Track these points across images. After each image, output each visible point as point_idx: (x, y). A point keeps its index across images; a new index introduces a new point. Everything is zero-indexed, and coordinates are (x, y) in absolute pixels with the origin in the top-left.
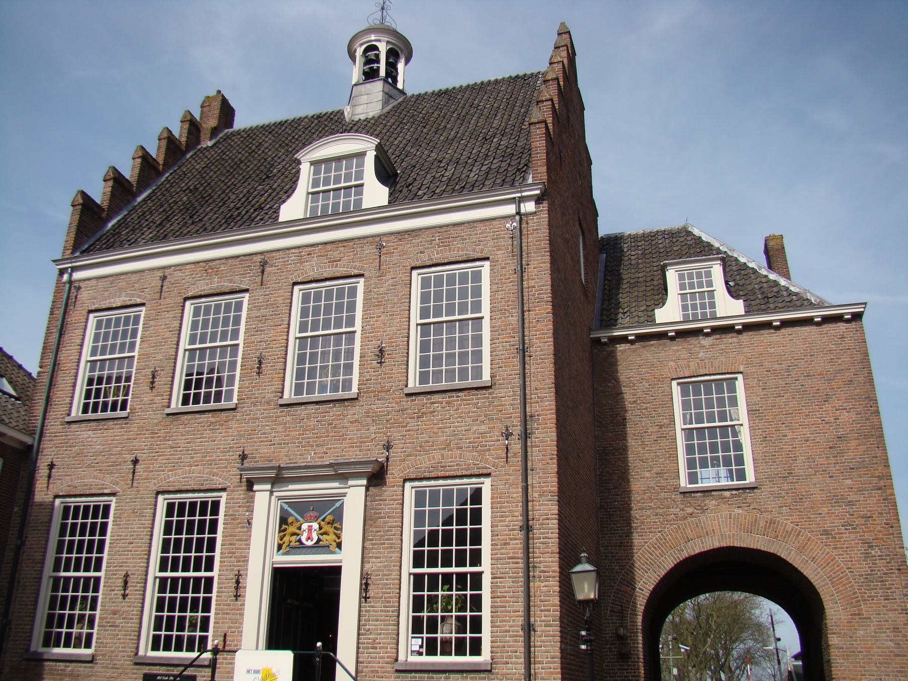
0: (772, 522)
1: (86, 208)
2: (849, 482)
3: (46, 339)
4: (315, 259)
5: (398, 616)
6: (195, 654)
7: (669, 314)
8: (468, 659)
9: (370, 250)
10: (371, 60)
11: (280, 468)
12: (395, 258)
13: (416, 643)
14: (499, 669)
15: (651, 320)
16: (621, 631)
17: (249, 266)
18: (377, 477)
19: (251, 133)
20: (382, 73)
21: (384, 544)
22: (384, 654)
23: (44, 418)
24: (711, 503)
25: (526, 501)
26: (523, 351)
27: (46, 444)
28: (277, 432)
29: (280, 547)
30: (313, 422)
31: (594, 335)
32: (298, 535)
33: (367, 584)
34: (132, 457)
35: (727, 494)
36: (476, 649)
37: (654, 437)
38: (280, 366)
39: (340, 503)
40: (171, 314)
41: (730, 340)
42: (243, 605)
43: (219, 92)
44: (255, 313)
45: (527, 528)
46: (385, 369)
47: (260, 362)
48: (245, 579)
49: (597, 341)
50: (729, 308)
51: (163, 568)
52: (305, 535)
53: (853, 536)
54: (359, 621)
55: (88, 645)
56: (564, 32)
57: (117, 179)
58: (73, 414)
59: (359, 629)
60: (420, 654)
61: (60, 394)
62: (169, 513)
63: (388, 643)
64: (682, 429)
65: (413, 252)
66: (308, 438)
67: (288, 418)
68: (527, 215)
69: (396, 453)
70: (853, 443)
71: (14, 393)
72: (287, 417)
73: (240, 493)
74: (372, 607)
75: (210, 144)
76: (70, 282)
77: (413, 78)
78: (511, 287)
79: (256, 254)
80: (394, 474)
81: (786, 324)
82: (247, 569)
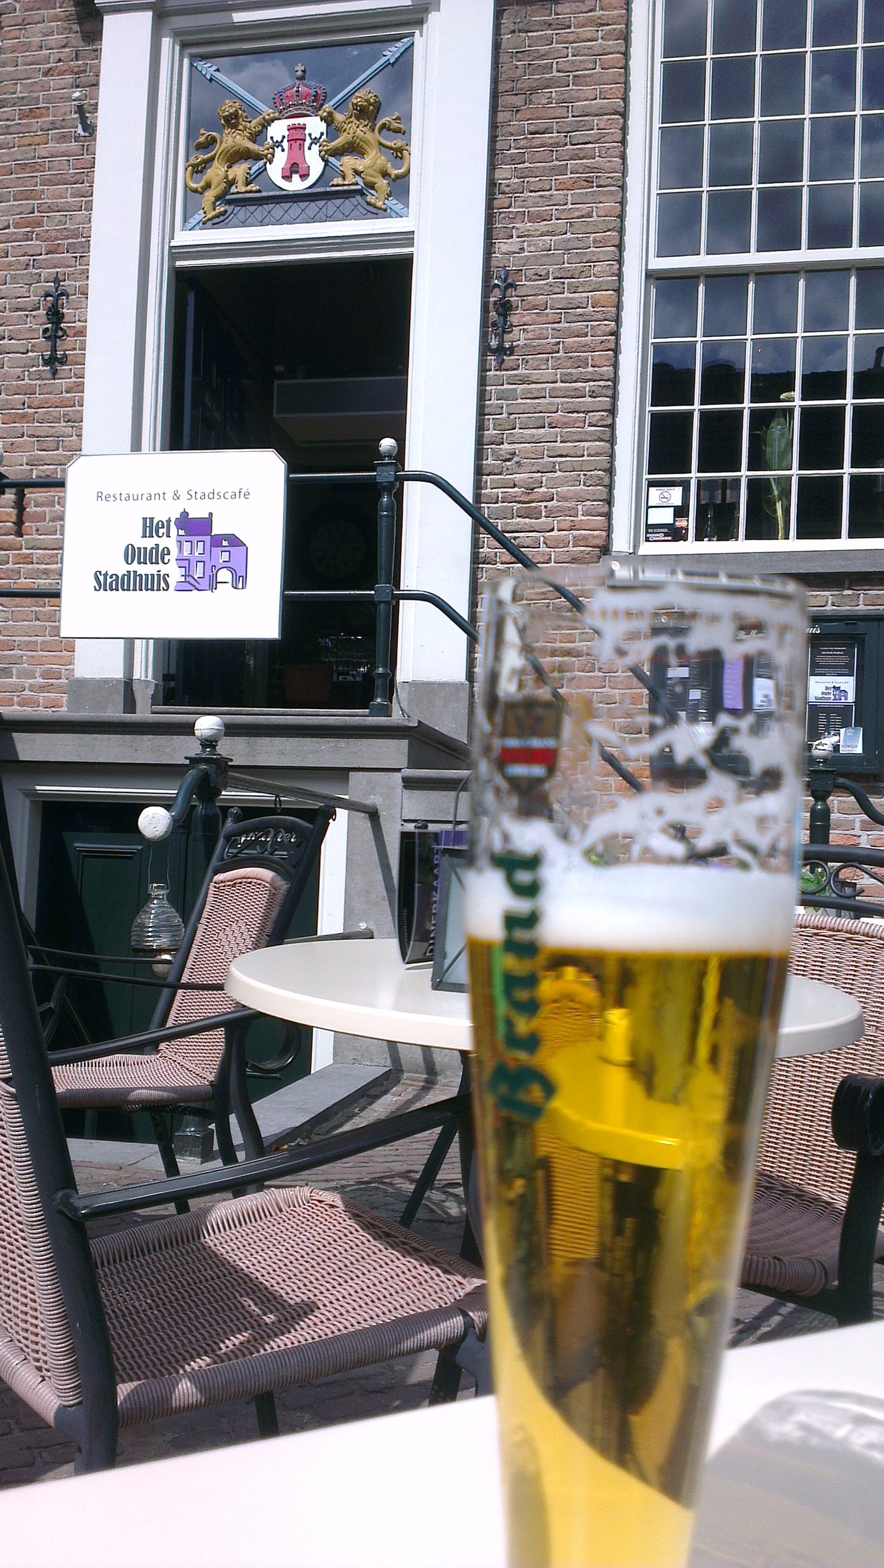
5: (613, 411)
13: (664, 503)
21: (562, 170)
32: (257, 157)
39: (401, 46)
42: (79, 387)
48: (82, 307)
52: (281, 158)
54: (481, 427)
59: (479, 454)
60: (676, 534)
64: (651, 276)
82: (85, 274)
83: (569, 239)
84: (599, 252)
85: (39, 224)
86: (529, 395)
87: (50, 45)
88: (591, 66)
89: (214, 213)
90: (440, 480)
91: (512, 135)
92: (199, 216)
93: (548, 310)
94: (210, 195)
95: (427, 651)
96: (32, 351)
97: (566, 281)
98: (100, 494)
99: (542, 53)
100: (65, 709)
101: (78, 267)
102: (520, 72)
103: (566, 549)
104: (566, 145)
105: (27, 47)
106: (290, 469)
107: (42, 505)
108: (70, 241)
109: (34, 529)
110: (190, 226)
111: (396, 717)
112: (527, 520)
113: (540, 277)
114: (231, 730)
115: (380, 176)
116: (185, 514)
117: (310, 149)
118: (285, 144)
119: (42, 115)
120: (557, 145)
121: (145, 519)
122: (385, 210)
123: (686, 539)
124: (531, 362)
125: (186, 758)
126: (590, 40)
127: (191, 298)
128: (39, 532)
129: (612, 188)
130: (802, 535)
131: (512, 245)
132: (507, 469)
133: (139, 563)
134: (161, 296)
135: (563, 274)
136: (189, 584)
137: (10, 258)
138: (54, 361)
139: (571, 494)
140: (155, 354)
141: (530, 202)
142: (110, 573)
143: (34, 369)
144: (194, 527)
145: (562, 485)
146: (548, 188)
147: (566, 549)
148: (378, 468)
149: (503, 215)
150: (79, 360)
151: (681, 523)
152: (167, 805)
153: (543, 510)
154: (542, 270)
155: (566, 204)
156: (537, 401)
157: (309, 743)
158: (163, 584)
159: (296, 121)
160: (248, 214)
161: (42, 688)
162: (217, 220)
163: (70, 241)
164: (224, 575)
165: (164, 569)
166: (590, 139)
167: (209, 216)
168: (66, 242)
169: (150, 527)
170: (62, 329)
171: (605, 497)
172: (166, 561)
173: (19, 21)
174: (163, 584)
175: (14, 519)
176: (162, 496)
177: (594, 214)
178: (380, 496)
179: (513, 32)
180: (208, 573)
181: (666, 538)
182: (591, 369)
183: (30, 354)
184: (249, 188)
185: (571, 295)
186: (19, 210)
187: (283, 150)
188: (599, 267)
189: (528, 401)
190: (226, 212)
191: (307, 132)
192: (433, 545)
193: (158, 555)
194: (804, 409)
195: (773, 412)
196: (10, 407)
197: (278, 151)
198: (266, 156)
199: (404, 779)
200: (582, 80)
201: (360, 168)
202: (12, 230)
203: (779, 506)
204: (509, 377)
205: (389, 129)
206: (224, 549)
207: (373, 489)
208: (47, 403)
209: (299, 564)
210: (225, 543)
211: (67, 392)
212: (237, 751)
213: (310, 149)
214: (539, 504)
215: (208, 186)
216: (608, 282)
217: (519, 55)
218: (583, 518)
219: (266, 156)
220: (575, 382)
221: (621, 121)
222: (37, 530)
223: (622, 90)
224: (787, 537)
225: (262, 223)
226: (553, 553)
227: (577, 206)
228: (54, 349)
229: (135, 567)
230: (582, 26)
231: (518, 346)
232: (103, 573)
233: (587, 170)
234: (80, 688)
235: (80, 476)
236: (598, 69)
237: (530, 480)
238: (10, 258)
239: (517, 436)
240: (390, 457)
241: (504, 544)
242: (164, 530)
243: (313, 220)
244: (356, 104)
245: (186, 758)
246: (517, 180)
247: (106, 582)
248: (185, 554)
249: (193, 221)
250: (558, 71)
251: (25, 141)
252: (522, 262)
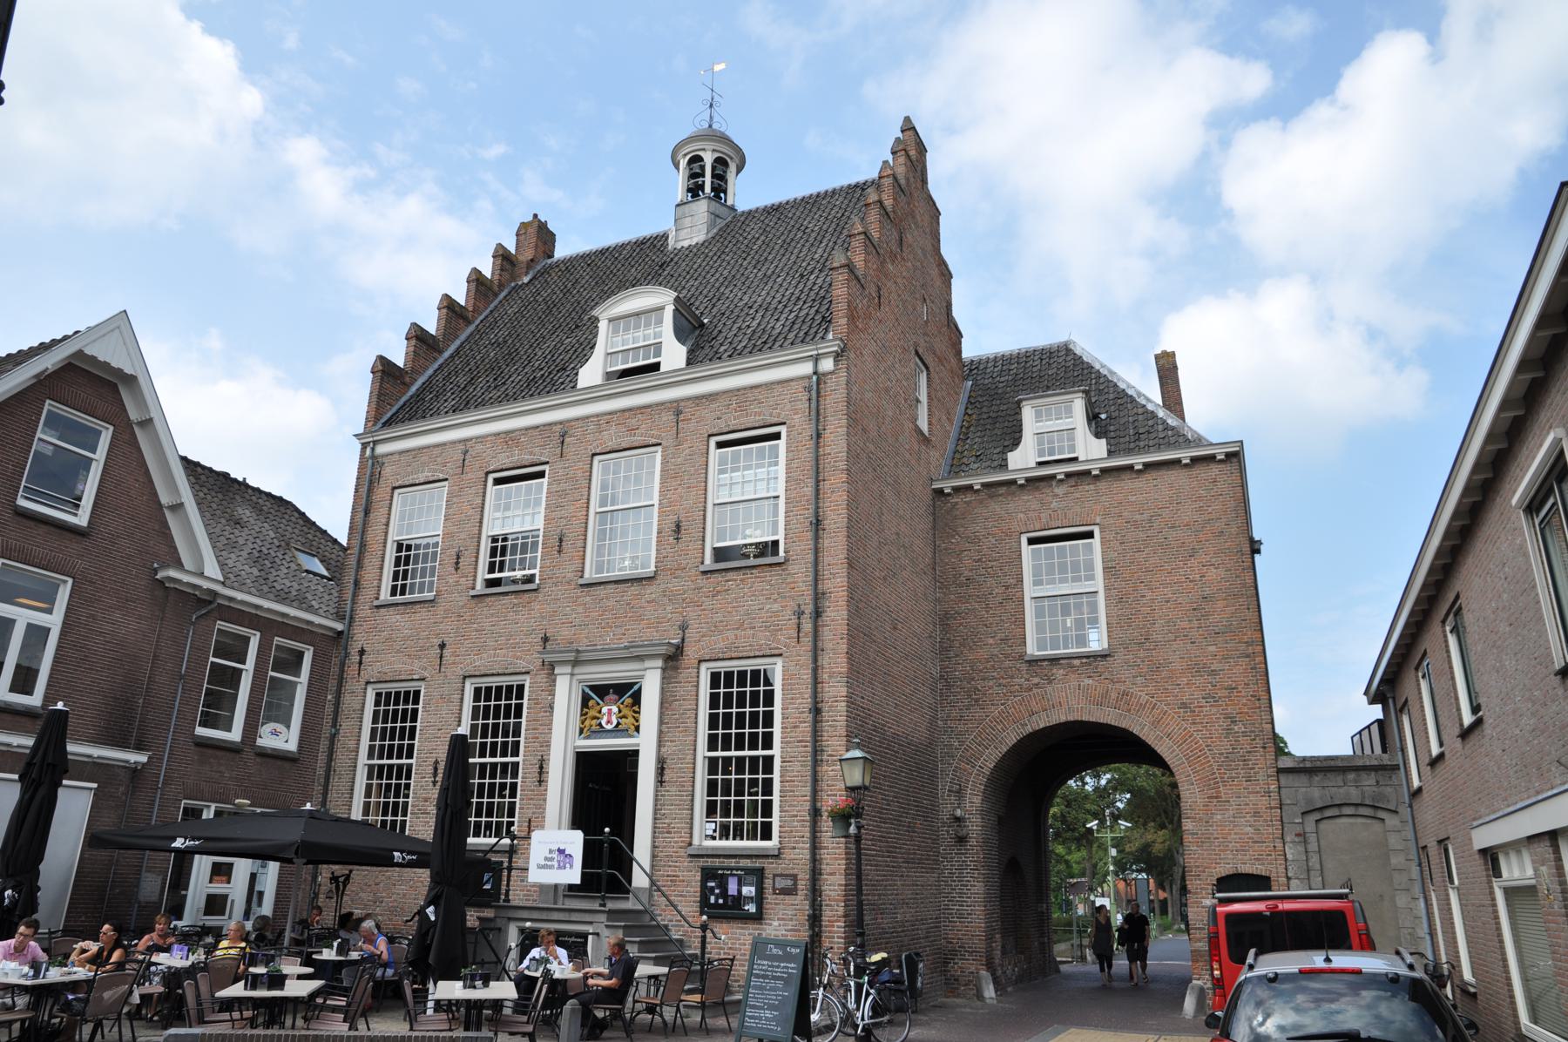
0: (1125, 694)
1: (385, 370)
2: (1212, 648)
3: (352, 519)
6: (493, 840)
7: (1023, 459)
8: (759, 843)
9: (668, 417)
10: (695, 175)
11: (578, 651)
12: (692, 425)
14: (788, 854)
15: (1003, 466)
16: (958, 813)
18: (673, 658)
19: (571, 263)
20: (708, 189)
22: (678, 839)
23: (354, 602)
24: (1059, 673)
25: (816, 681)
26: (817, 524)
27: (356, 630)
29: (581, 731)
30: (611, 603)
31: (936, 486)
33: (662, 769)
34: (437, 641)
35: (1077, 662)
36: (767, 835)
37: (999, 599)
38: (580, 544)
40: (473, 491)
41: (1088, 488)
43: (535, 216)
44: (555, 488)
45: (816, 711)
46: (682, 545)
47: (561, 540)
49: (940, 492)
50: (1092, 450)
51: (712, 745)
53: (1214, 710)
55: (767, 835)
56: (908, 127)
57: (418, 336)
58: (382, 597)
60: (714, 838)
61: (368, 574)
62: (477, 698)
65: (709, 419)
68: (824, 374)
69: (691, 634)
70: (1220, 604)
71: (325, 573)
73: (542, 678)
75: (526, 280)
76: (373, 457)
77: (747, 193)
78: (807, 454)
79: (555, 424)
80: (691, 653)
81: (1147, 466)
136: (559, 868)
144: (561, 851)
157: (826, 559)
169: (551, 851)
193: (552, 859)
209: (586, 863)
247: (540, 867)
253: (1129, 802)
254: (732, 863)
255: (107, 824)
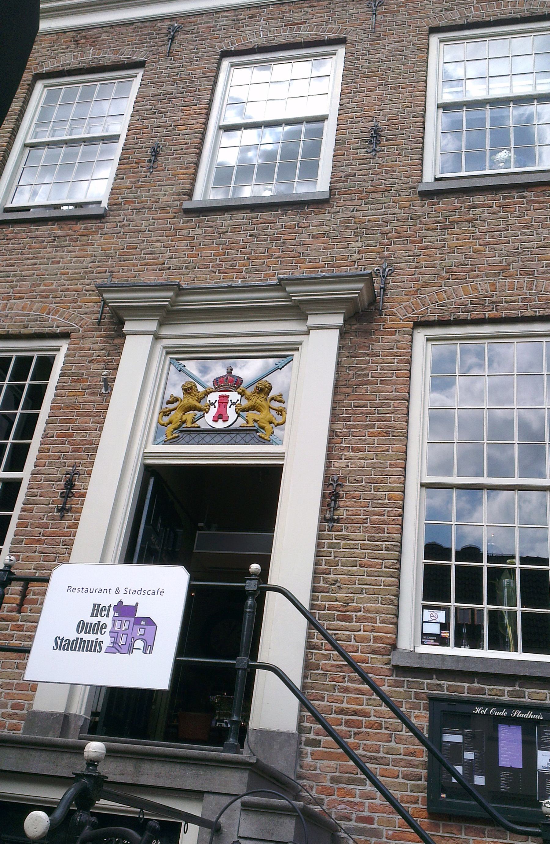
4: (262, 22)
11: (180, 290)
17: (149, 34)
18: (362, 318)
21: (373, 426)
28: (176, 251)
30: (242, 237)
38: (192, 158)
42: (76, 526)
52: (213, 411)
63: (378, 612)
66: (233, 260)
67: (198, 231)
72: (197, 230)
73: (95, 343)
74: (345, 538)
80: (398, 307)
83: (375, 462)
84: (393, 471)
85: (71, 436)
86: (348, 547)
87: (95, 349)
88: (390, 376)
89: (171, 437)
90: (286, 591)
91: (344, 407)
92: (164, 438)
93: (361, 500)
94: (171, 427)
95: (273, 708)
96: (52, 504)
97: (373, 485)
98: (70, 588)
99: (363, 368)
100: (21, 732)
101: (89, 460)
102: (351, 376)
103: (369, 644)
104: (375, 414)
105: (82, 349)
106: (191, 579)
107: (37, 594)
108: (87, 446)
109: (29, 609)
110: (157, 443)
111: (245, 755)
112: (343, 623)
113: (357, 481)
114: (111, 753)
115: (268, 423)
116: (121, 602)
117: (230, 407)
118: (217, 404)
119: (84, 382)
120: (370, 413)
121: (95, 605)
122: (269, 441)
123: (449, 646)
124: (350, 528)
125: (73, 773)
126: (390, 363)
127: (152, 481)
128: (32, 611)
129: (401, 438)
130: (525, 650)
131: (342, 463)
132: (332, 590)
133: (85, 633)
134: (134, 478)
135: (371, 481)
136: (115, 648)
137: (50, 453)
138: (63, 510)
139: (373, 609)
140: (125, 509)
141: (353, 442)
142: (65, 639)
143: (51, 514)
144: (125, 611)
145: (367, 603)
146: (364, 435)
147: (369, 644)
148: (247, 581)
149: (337, 448)
150: (79, 510)
151: (445, 634)
152: (49, 811)
153: (354, 617)
154: (358, 478)
155: (374, 444)
156: (353, 550)
158: (98, 648)
159: (224, 393)
160: (191, 438)
161: (10, 716)
162: (171, 441)
163: (87, 446)
164: (139, 644)
165: (100, 637)
166: (389, 412)
167: (169, 438)
168: (84, 446)
169: (97, 610)
170: (72, 492)
171: (394, 612)
172: (103, 633)
173: (81, 336)
174: (98, 648)
175: (18, 602)
176: (108, 590)
177: (390, 450)
178: (246, 599)
179: (348, 357)
180: (129, 642)
181: (435, 643)
182: (386, 535)
183: (50, 505)
184: (193, 425)
185: (375, 493)
186: (61, 428)
187: (215, 407)
188: (393, 478)
189: (347, 550)
190: (178, 436)
191: (229, 399)
192: (282, 636)
193: (99, 628)
194: (522, 570)
195: (502, 570)
196: (31, 535)
197: (212, 407)
198: (205, 410)
199: (244, 804)
200: (384, 382)
201: (257, 419)
202: (55, 438)
203: (509, 630)
204: (336, 536)
205: (275, 401)
206: (142, 627)
207: (243, 594)
208: (54, 534)
209: (187, 642)
210: (143, 623)
211: (67, 528)
212: (113, 771)
213: (230, 407)
214: (352, 613)
215: (170, 423)
216: (397, 487)
217: (351, 368)
218: (380, 625)
219: (205, 410)
220: (376, 541)
221: (407, 404)
222: (31, 610)
223: (408, 389)
224: (516, 650)
225: (198, 444)
226: (360, 647)
227: (380, 445)
228: (65, 503)
229: (83, 635)
230: (386, 356)
231: (342, 518)
232: (61, 638)
233: (387, 427)
234: (34, 718)
235: (61, 576)
236: (394, 378)
237: (346, 598)
238: (50, 453)
239: (339, 570)
240: (255, 575)
241: (326, 637)
242: (106, 613)
243: (228, 443)
244: (258, 387)
245: (73, 773)
246: (346, 430)
247: (62, 644)
248: (116, 629)
249: (159, 441)
250: (372, 377)
251: (72, 394)
252: (347, 472)
253: (213, 694)
254: (505, 694)
255: (72, 719)
